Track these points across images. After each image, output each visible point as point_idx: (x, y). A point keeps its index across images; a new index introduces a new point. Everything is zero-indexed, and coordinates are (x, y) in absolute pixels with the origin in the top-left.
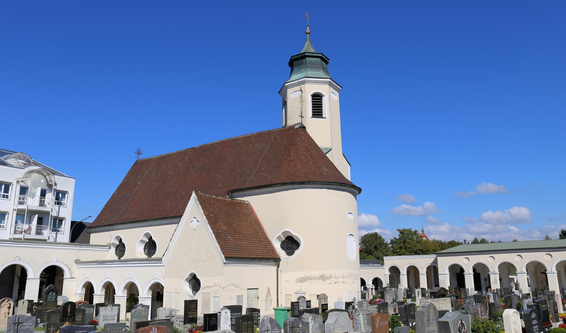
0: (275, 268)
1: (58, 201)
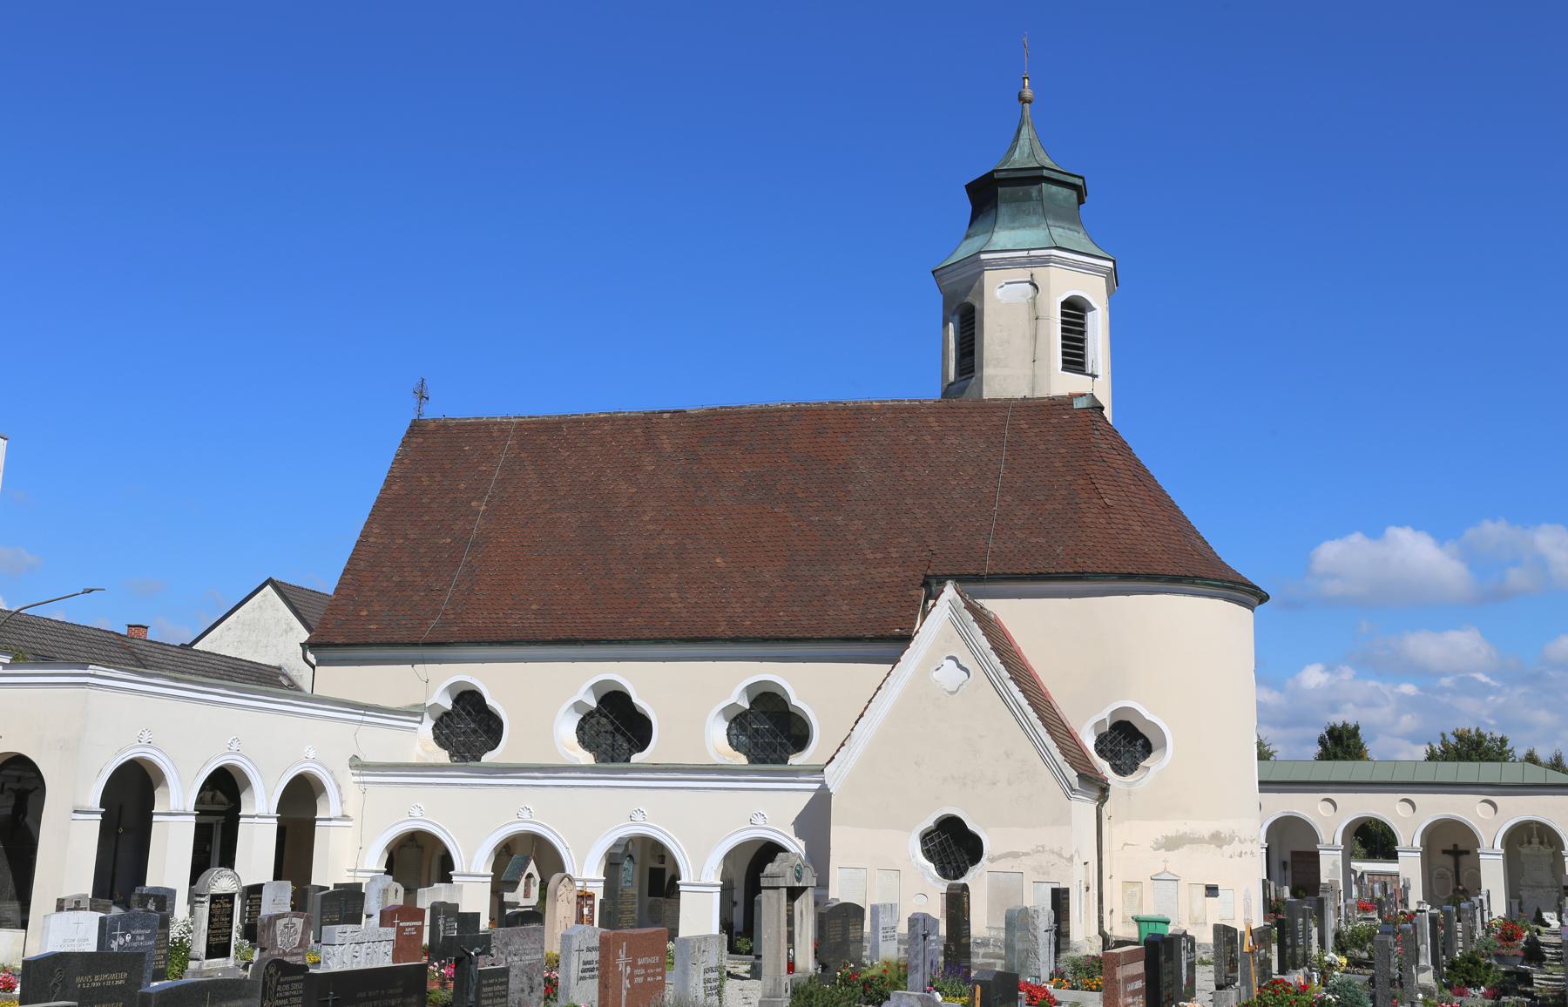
0: (1093, 807)
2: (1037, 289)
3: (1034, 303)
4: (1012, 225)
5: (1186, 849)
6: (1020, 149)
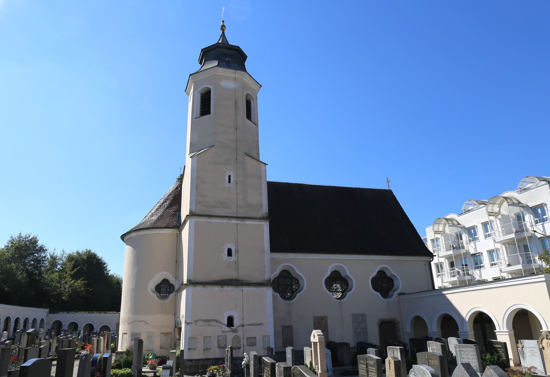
1: (540, 218)
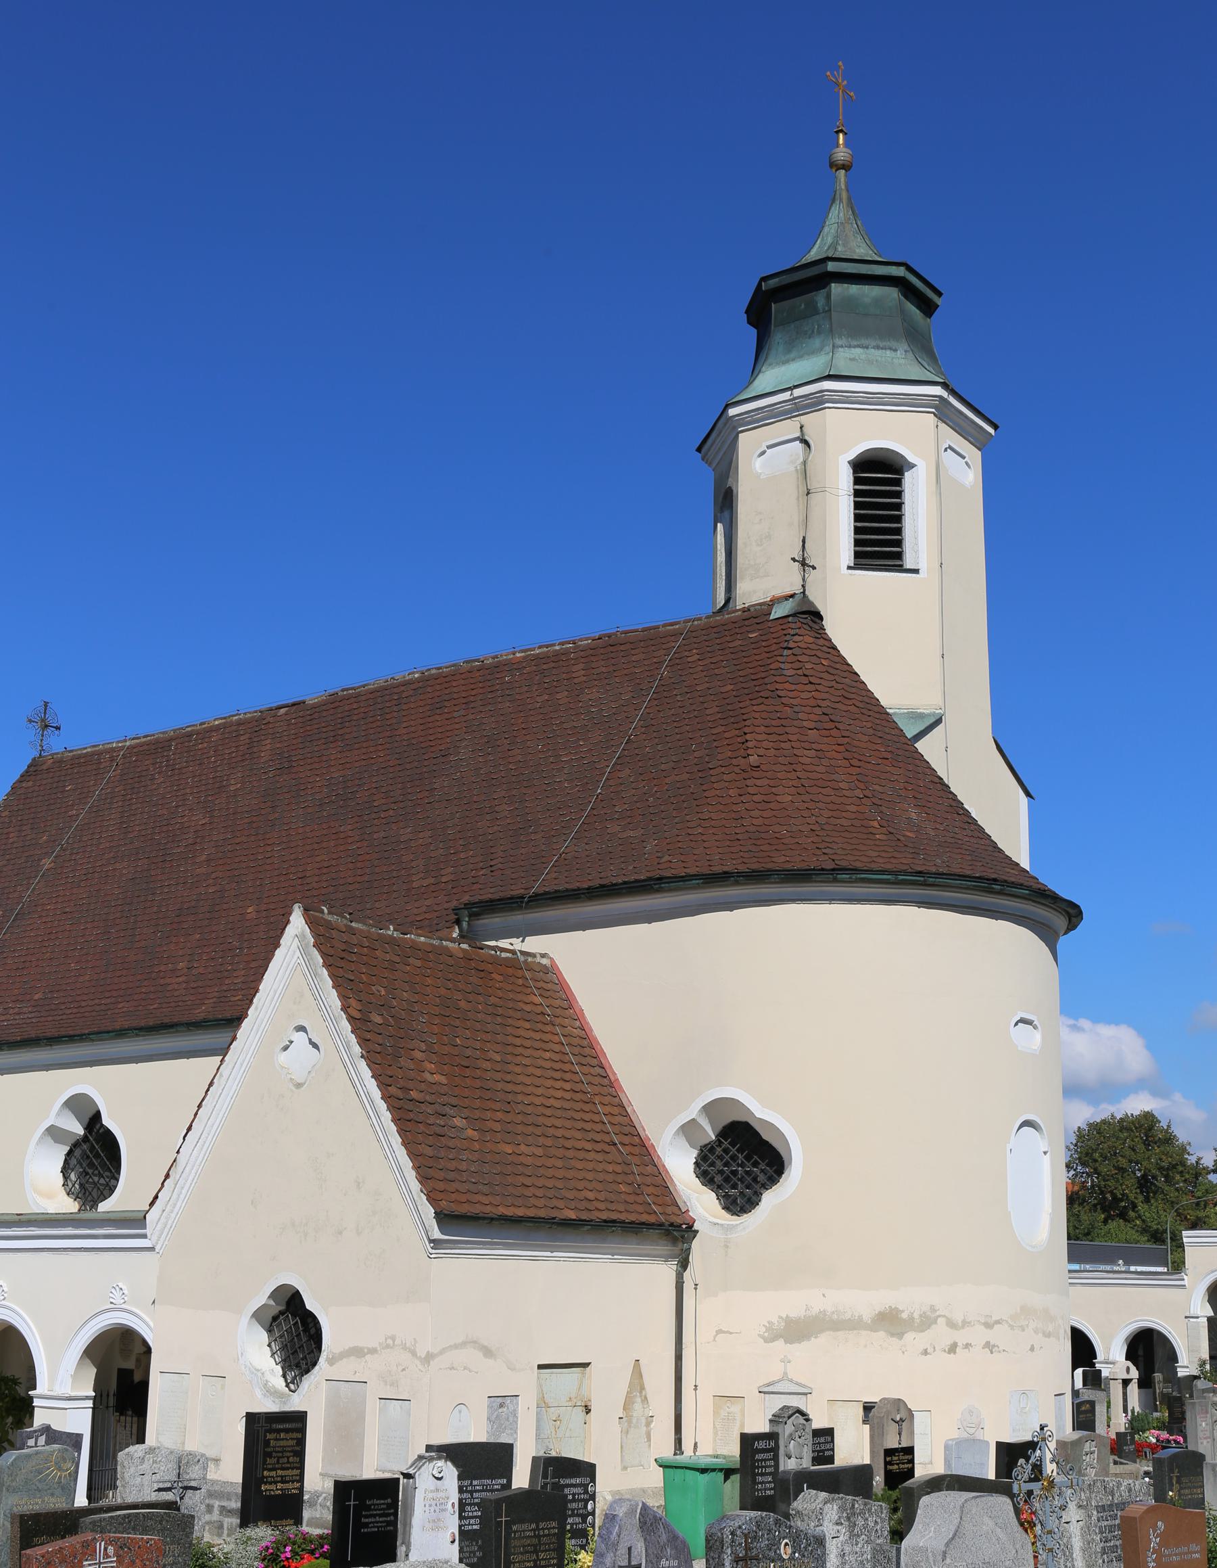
2: (809, 446)
3: (804, 471)
4: (788, 356)
5: (824, 1339)
6: (823, 240)
